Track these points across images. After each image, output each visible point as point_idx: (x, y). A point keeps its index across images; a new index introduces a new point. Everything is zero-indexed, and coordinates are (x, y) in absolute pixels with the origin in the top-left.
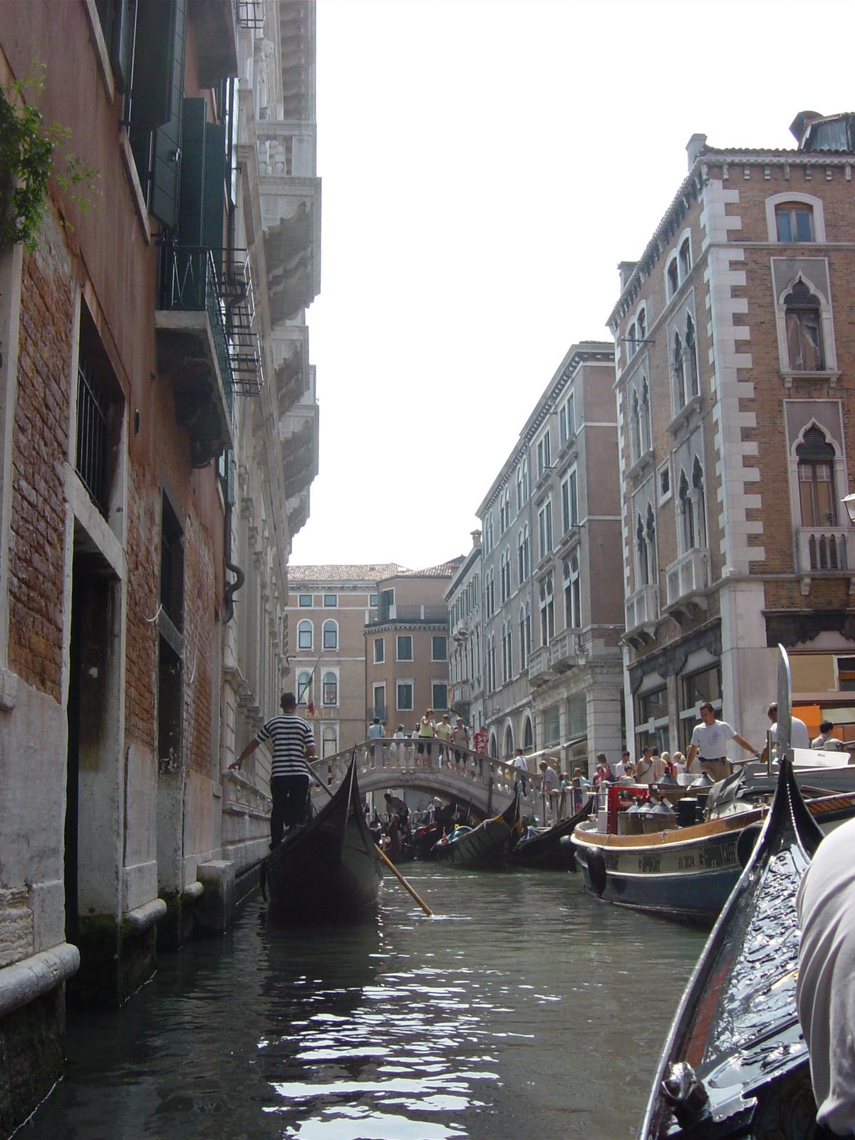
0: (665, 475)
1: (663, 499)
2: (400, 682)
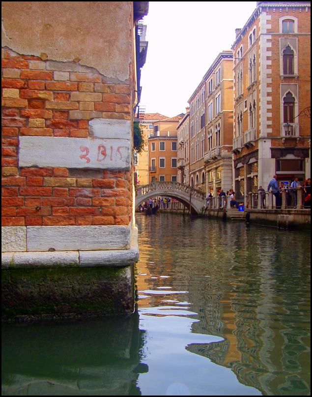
0: (246, 102)
1: (245, 110)
2: (160, 158)
